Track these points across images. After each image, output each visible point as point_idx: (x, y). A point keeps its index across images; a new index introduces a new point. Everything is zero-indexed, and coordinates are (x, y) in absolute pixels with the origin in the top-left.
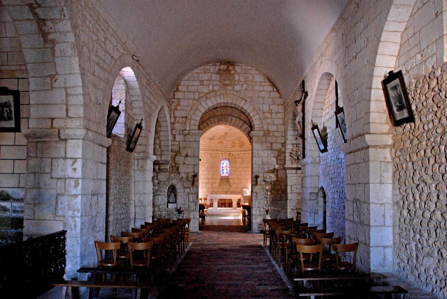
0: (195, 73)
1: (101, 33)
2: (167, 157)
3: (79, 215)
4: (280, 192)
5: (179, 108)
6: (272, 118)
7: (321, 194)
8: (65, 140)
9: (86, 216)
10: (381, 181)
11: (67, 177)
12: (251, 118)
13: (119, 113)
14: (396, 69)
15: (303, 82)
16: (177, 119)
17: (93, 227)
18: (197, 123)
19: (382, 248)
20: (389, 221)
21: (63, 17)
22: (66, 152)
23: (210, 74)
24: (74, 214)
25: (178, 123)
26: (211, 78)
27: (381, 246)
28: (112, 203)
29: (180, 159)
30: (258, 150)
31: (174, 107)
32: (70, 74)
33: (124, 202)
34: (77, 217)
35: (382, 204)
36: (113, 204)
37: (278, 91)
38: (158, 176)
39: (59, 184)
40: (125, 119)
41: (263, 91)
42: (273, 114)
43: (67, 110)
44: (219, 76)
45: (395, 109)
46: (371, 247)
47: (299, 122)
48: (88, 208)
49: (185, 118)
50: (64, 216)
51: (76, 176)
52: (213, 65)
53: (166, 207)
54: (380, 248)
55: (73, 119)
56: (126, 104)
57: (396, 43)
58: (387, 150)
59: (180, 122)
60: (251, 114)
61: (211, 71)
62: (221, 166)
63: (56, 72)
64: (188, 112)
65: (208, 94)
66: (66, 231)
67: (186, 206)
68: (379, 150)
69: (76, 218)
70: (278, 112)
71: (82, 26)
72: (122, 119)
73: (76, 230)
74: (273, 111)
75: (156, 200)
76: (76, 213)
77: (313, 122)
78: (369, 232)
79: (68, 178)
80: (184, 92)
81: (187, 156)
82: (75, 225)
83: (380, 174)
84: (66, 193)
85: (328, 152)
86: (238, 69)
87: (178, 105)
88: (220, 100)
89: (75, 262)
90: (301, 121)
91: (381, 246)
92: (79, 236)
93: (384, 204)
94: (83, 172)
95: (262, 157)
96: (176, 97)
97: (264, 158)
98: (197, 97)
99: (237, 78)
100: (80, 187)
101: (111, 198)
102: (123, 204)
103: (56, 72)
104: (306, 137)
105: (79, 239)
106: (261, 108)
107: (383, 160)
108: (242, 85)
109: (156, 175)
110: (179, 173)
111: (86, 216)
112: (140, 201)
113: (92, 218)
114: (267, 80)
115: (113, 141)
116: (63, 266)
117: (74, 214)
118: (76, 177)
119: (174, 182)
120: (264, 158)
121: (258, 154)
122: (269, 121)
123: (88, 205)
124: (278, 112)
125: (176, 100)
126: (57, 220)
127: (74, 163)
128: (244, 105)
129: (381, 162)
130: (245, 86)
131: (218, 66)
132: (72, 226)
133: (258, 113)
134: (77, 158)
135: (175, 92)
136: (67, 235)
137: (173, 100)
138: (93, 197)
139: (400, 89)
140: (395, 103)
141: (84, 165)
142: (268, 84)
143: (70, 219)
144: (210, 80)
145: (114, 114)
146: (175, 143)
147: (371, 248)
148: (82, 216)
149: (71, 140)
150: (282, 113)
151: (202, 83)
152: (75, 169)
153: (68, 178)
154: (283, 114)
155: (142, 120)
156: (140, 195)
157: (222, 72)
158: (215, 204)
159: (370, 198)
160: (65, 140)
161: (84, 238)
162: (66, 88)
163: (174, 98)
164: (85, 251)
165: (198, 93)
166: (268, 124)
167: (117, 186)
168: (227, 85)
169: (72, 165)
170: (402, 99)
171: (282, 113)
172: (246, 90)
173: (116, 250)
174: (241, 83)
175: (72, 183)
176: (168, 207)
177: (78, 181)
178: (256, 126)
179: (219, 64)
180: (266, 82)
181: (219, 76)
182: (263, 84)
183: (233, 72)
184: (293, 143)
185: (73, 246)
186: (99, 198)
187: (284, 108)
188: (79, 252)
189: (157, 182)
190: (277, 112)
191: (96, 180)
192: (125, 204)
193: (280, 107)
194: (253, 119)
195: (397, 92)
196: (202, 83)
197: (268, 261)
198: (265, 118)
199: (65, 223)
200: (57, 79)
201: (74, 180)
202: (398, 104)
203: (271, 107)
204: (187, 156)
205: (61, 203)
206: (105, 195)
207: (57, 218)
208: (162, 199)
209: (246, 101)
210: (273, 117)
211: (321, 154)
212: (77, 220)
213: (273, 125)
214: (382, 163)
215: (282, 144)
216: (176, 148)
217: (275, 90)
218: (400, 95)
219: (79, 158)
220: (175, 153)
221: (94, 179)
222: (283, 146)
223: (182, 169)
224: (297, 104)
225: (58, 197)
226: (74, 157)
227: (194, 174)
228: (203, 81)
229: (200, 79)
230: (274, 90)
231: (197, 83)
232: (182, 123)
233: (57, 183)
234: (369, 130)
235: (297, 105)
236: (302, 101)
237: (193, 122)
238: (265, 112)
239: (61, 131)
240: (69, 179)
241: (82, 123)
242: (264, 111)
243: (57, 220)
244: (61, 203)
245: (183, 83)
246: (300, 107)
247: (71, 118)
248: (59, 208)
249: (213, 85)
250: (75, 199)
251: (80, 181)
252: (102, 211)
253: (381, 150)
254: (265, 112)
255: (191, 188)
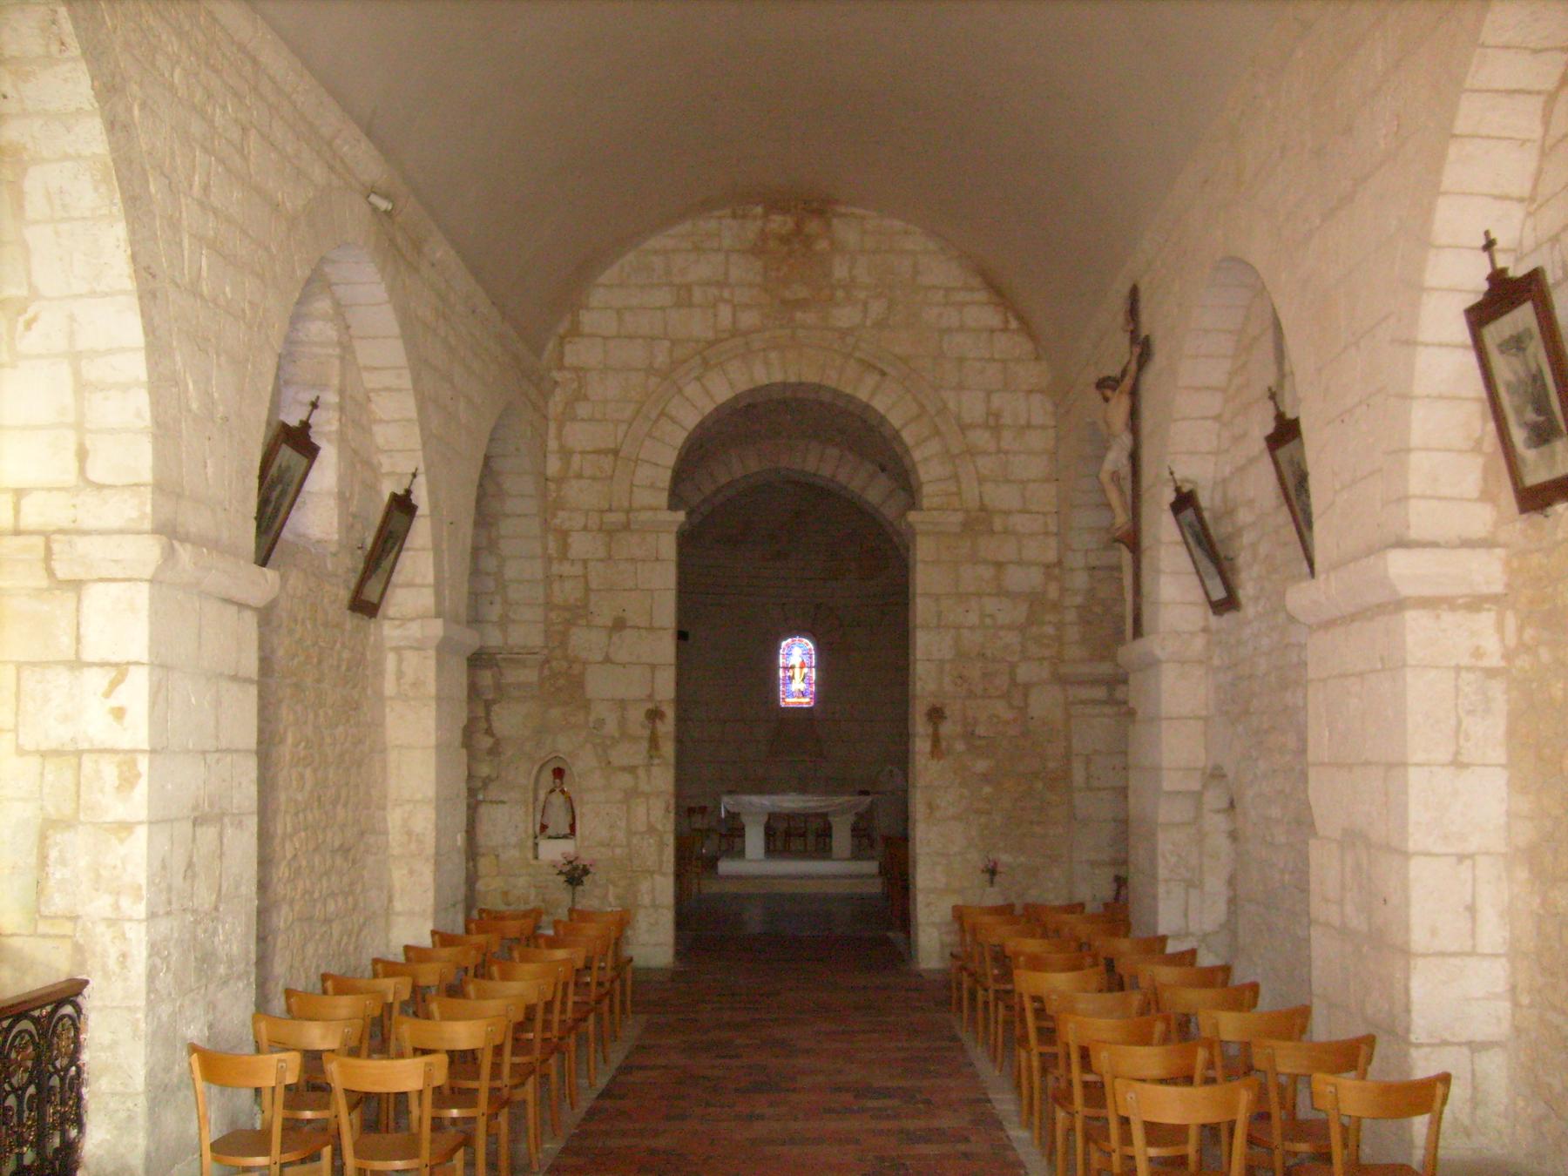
0: (656, 252)
1: (224, 107)
2: (526, 633)
3: (141, 910)
4: (1039, 785)
5: (583, 410)
6: (999, 451)
7: (1215, 798)
8: (77, 585)
9: (168, 913)
10: (1457, 753)
11: (86, 746)
12: (907, 451)
13: (310, 452)
14: (1518, 260)
15: (1134, 293)
16: (576, 461)
17: (204, 960)
18: (665, 478)
19: (1465, 1050)
20: (1493, 933)
21: (54, 48)
22: (78, 639)
23: (721, 257)
24: (116, 907)
25: (579, 476)
26: (726, 274)
27: (1460, 1044)
28: (286, 850)
29: (586, 641)
30: (937, 598)
31: (560, 409)
32: (93, 294)
33: (337, 844)
34: (130, 920)
35: (1461, 858)
36: (289, 856)
37: (1027, 327)
38: (494, 717)
39: (50, 777)
40: (341, 478)
41: (962, 328)
42: (1007, 435)
43: (82, 455)
44: (758, 264)
45: (1518, 436)
46: (1419, 1046)
47: (1115, 476)
48: (178, 881)
49: (611, 457)
50: (74, 918)
51: (125, 742)
52: (734, 216)
53: (530, 855)
54: (1454, 1049)
55: (107, 492)
56: (341, 409)
57: (1524, 142)
58: (1486, 619)
59: (587, 472)
60: (905, 435)
61: (727, 243)
62: (781, 661)
63: (30, 285)
64: (623, 427)
65: (711, 344)
66: (87, 982)
67: (618, 851)
68: (1448, 618)
69: (127, 925)
70: (1029, 426)
71: (141, 85)
72: (324, 476)
73: (126, 979)
74: (1007, 420)
75: (484, 827)
76: (125, 903)
77: (1177, 476)
78: (1407, 979)
79: (90, 751)
80: (605, 338)
81: (619, 625)
82: (124, 956)
83: (1453, 722)
84: (82, 817)
85: (1241, 615)
86: (847, 233)
87: (580, 396)
88: (765, 372)
89: (122, 1115)
90: (1126, 470)
91: (1460, 1044)
92: (142, 1003)
93: (1471, 856)
94: (158, 721)
95: (957, 628)
96: (569, 360)
97: (965, 632)
98: (661, 359)
99: (840, 271)
100: (142, 789)
101: (283, 824)
102: (334, 852)
103: (30, 285)
104: (1146, 542)
105: (140, 1015)
106: (952, 405)
107: (1466, 661)
108: (865, 304)
109: (481, 712)
110: (586, 705)
111: (168, 913)
112: (409, 833)
113: (197, 923)
114: (976, 282)
115: (284, 579)
116: (73, 1133)
117: (116, 907)
118: (127, 746)
119: (563, 744)
120: (965, 632)
121: (939, 613)
122: (985, 464)
123: (179, 863)
124: (1029, 426)
125: (568, 375)
126: (44, 936)
127: (115, 684)
128: (873, 395)
129: (1458, 669)
130: (877, 308)
131: (755, 218)
132: (112, 964)
133: (937, 432)
134: (128, 663)
135: (562, 338)
136: (91, 1001)
137: (556, 375)
138: (199, 831)
139: (1537, 351)
140: (1519, 412)
141: (158, 695)
142: (982, 296)
143: (101, 928)
144: (721, 285)
145: (287, 454)
146: (566, 569)
147: (1414, 1052)
148: (152, 916)
149: (101, 585)
150: (1043, 427)
151: (684, 297)
152: (119, 713)
153: (90, 751)
154: (1051, 433)
155: (414, 475)
156: (408, 807)
157: (772, 244)
158: (754, 840)
159: (1411, 829)
160: (77, 585)
161: (165, 1010)
162: (76, 357)
163: (561, 368)
164: (167, 1070)
165: (667, 344)
166: (981, 480)
167: (308, 773)
168: (802, 304)
169: (107, 695)
170: (1547, 396)
171: (1043, 427)
172: (881, 325)
173: (280, 1092)
174: (862, 295)
175: (110, 770)
176: (536, 858)
177: (134, 764)
178: (927, 489)
179: (759, 210)
180: (972, 289)
181: (758, 264)
182: (959, 297)
183: (822, 245)
184: (1093, 561)
185: (114, 1045)
186: (229, 831)
187: (1056, 405)
188: (142, 1073)
189: (487, 742)
190: (1023, 422)
191: (211, 758)
192: (345, 850)
193: (1036, 399)
194: (917, 455)
195: (1526, 364)
196: (684, 297)
197: (978, 1101)
198: (972, 452)
199: (78, 949)
200: (34, 319)
201: (117, 758)
202: (1531, 416)
203: (996, 400)
204: (619, 625)
205: (63, 862)
206: (255, 819)
207: (43, 927)
208: (506, 824)
209: (883, 374)
210: (1004, 445)
211: (1214, 620)
212: (131, 934)
213: (1008, 481)
214: (1463, 674)
215: (1047, 566)
216: (568, 592)
217: (1014, 324)
218: (1537, 378)
219: (137, 663)
220: (567, 615)
221: (204, 752)
222: (1049, 576)
223: (600, 685)
224: (1109, 393)
225: (50, 832)
226: (114, 659)
227: (650, 706)
228: (688, 287)
229: (677, 280)
230: (1007, 322)
231: (663, 297)
232: (594, 478)
233: (42, 774)
234: (1408, 527)
235: (1106, 400)
236: (1128, 381)
237: (644, 473)
238: (972, 426)
239: (56, 547)
240: (94, 757)
241: (148, 509)
242: (967, 419)
243: (44, 936)
244: (63, 862)
245: (597, 297)
246: (1119, 408)
247: (100, 487)
248: (52, 882)
249: (734, 307)
250: (122, 841)
251: (143, 764)
252: (243, 890)
253: (1460, 616)
254: (972, 426)
255: (641, 772)
